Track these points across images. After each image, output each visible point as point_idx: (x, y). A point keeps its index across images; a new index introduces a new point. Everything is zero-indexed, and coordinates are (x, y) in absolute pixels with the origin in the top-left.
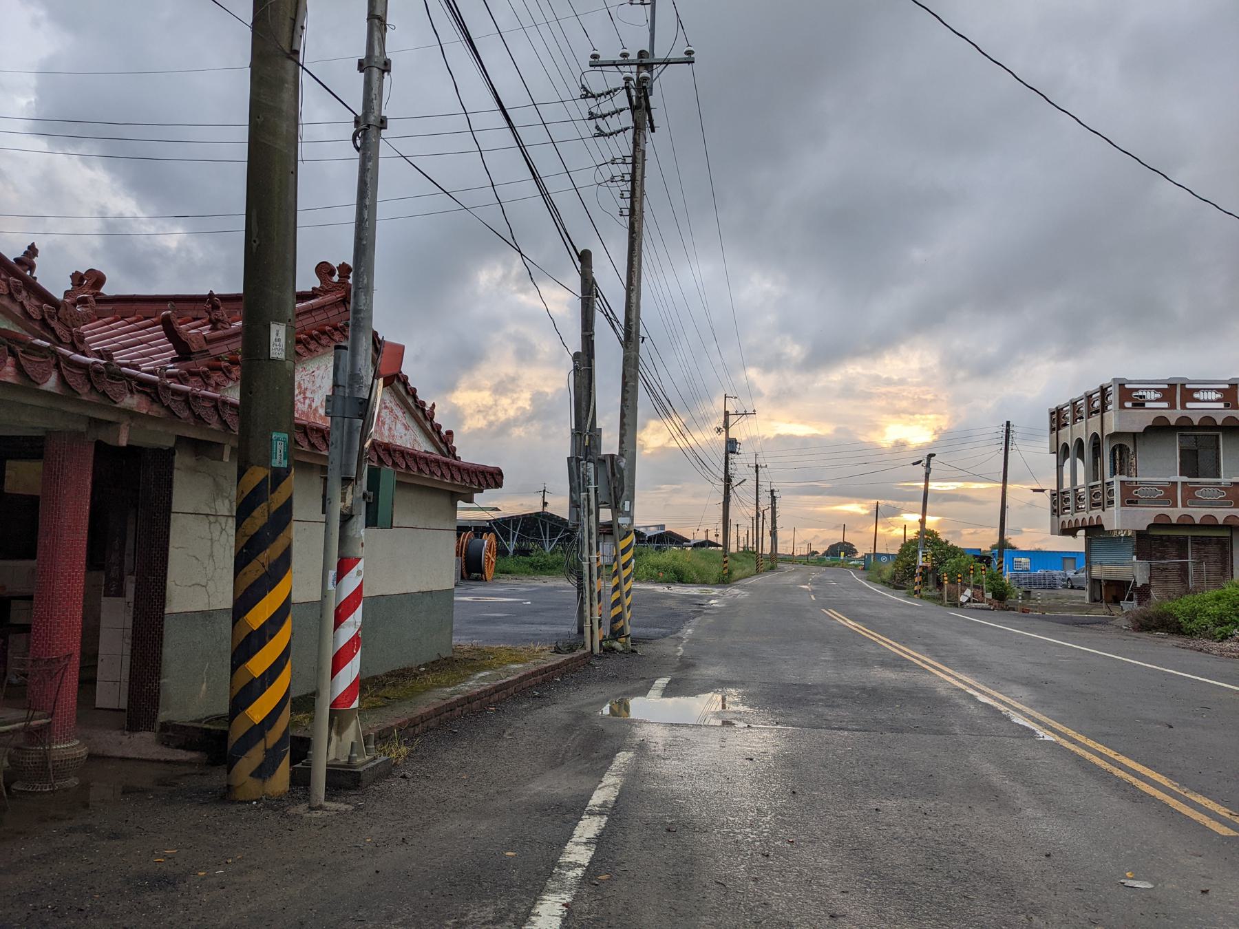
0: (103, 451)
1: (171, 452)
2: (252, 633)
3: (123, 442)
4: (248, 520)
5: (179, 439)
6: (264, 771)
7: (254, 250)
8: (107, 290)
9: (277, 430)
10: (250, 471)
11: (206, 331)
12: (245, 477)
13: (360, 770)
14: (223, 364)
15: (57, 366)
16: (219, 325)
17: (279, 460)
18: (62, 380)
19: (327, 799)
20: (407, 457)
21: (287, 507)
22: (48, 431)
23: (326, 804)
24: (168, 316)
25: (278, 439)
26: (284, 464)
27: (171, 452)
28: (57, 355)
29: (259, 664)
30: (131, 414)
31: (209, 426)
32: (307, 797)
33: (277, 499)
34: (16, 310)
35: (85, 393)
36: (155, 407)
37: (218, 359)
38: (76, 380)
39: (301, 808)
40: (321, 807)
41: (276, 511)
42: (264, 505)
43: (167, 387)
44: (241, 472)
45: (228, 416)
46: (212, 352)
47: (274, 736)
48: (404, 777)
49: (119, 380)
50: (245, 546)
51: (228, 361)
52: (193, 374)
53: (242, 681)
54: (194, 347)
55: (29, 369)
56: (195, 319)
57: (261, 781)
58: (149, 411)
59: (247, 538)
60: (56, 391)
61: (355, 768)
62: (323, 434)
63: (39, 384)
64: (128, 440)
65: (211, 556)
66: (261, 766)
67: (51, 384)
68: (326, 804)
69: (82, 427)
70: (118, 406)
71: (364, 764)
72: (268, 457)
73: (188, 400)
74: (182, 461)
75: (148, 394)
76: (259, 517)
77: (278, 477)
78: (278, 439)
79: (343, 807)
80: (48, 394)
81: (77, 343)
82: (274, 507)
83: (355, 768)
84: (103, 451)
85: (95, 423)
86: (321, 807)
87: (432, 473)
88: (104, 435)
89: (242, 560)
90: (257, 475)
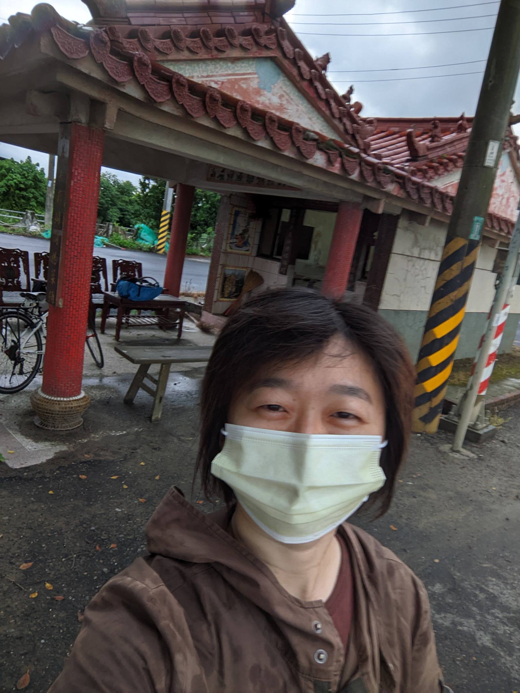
0: (368, 215)
1: (398, 217)
2: (437, 340)
3: (380, 211)
4: (448, 270)
5: (404, 210)
6: (427, 419)
7: (489, 88)
8: (363, 114)
9: (478, 215)
10: (455, 240)
11: (427, 142)
12: (452, 243)
13: (481, 432)
14: (435, 164)
15: (360, 164)
16: (436, 139)
17: (475, 236)
18: (361, 173)
19: (463, 447)
20: (495, 220)
21: (471, 268)
22: (342, 202)
23: (462, 450)
24: (410, 133)
25: (477, 221)
26: (477, 238)
27: (398, 217)
28: (362, 160)
29: (435, 359)
30: (388, 195)
31: (192, 119)
32: (452, 441)
33: (467, 261)
34: (341, 127)
35: (370, 182)
36: (402, 192)
37: (432, 161)
38: (367, 173)
39: (446, 447)
40: (458, 452)
41: (466, 268)
42: (459, 263)
43: (410, 179)
44: (449, 240)
45: (449, 205)
46: (430, 156)
47: (437, 401)
48: (503, 442)
49: (387, 174)
50: (442, 287)
51: (438, 163)
52: (420, 170)
53: (423, 366)
54: (421, 152)
55: (347, 165)
56: (382, 132)
57: (424, 424)
58: (398, 194)
59: (445, 282)
60: (356, 179)
61: (478, 430)
62: (513, 225)
63: (254, 140)
64: (384, 210)
65: (405, 280)
66: (426, 416)
67: (355, 176)
68: (462, 450)
69: (359, 200)
70: (384, 190)
71: (482, 429)
72: (469, 233)
73: (419, 187)
74: (402, 223)
75: (399, 183)
76: (455, 270)
77: (472, 246)
78: (477, 221)
79: (472, 455)
80: (353, 181)
81: (366, 149)
82: (466, 265)
83: (478, 430)
84: (368, 215)
85: (367, 198)
86: (458, 452)
87: (501, 230)
88: (370, 206)
89: (437, 295)
90: (459, 243)
